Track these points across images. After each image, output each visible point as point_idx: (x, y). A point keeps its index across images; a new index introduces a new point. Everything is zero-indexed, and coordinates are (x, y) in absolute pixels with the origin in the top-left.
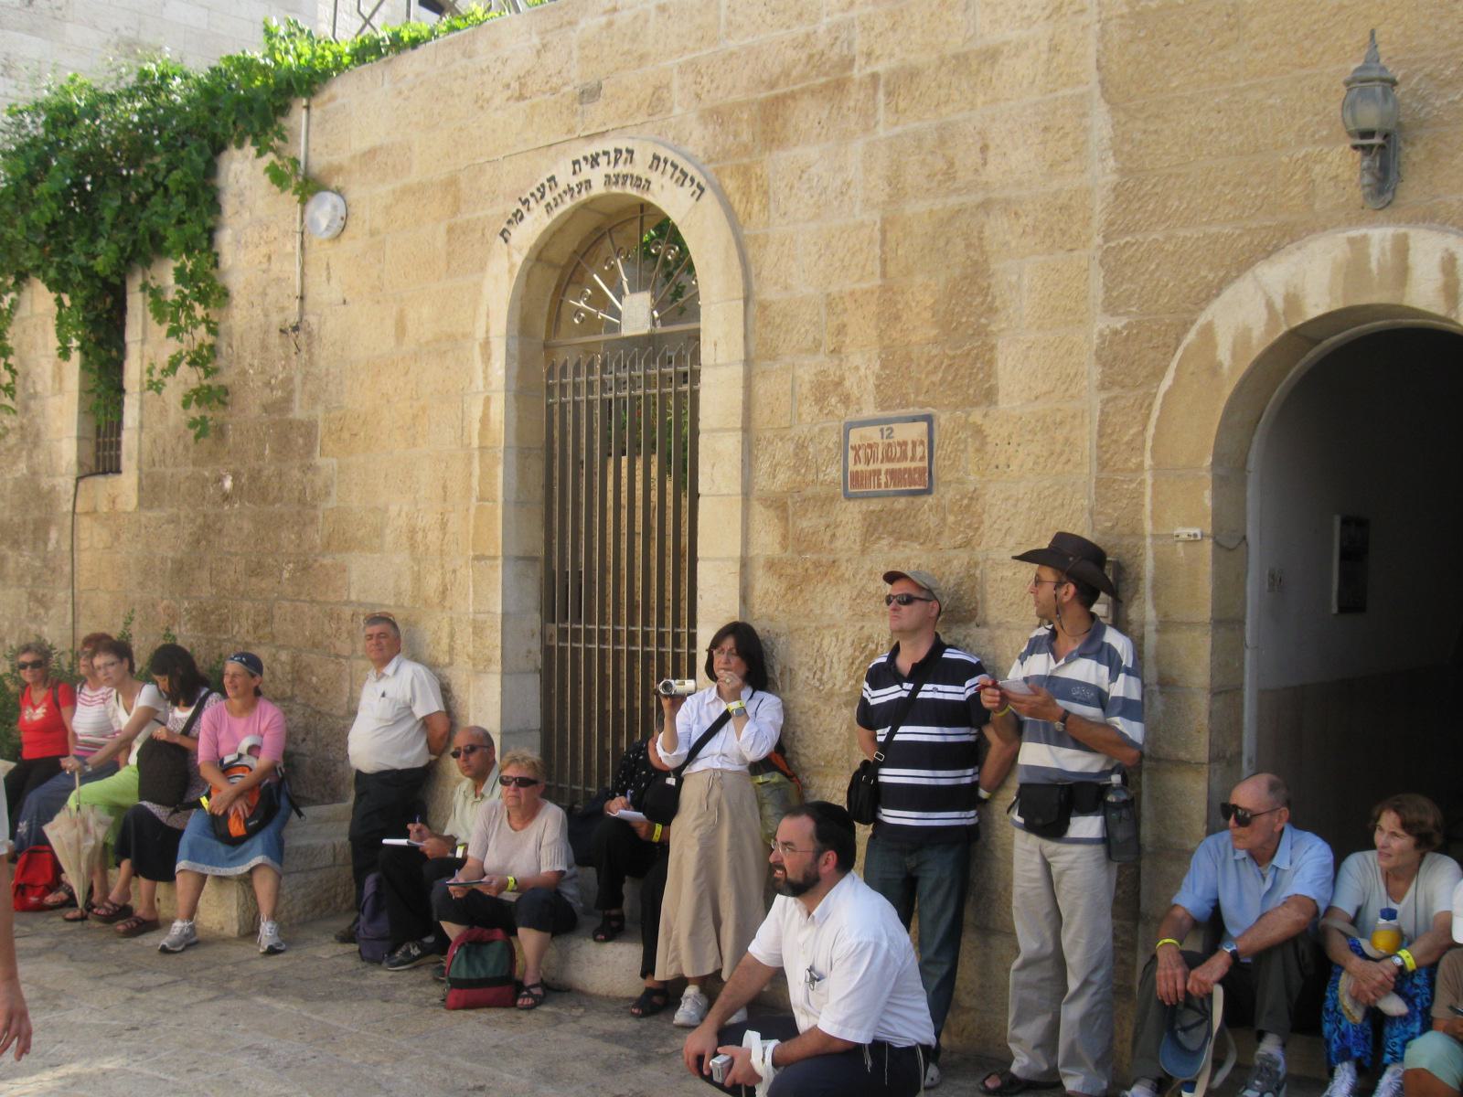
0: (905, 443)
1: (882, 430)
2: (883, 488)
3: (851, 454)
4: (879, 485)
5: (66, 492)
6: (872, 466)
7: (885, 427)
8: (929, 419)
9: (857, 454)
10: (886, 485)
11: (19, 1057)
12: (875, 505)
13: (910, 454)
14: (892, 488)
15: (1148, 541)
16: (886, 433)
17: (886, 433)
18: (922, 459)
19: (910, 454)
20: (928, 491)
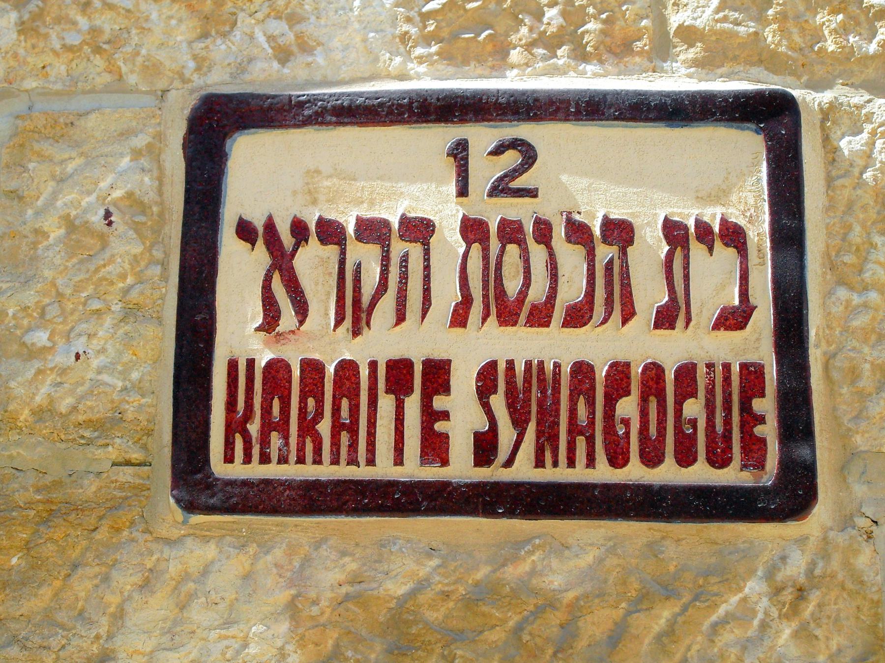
0: (620, 232)
1: (460, 153)
2: (461, 467)
3: (240, 271)
4: (435, 447)
5: (653, 549)
6: (384, 341)
7: (481, 137)
8: (770, 114)
9: (281, 262)
10: (485, 447)
11: (625, 321)
12: (410, 555)
13: (650, 293)
14: (524, 470)
15: (735, 599)
16: (485, 171)
17: (485, 171)
18: (734, 319)
19: (650, 293)
20: (793, 494)
